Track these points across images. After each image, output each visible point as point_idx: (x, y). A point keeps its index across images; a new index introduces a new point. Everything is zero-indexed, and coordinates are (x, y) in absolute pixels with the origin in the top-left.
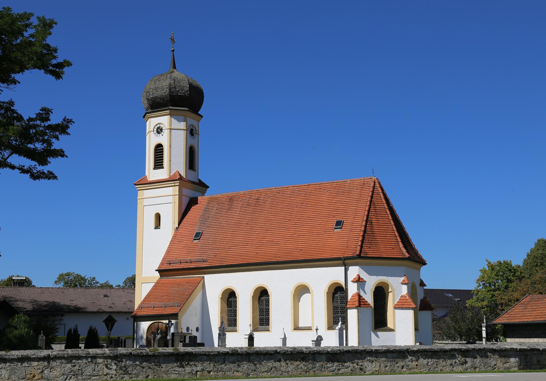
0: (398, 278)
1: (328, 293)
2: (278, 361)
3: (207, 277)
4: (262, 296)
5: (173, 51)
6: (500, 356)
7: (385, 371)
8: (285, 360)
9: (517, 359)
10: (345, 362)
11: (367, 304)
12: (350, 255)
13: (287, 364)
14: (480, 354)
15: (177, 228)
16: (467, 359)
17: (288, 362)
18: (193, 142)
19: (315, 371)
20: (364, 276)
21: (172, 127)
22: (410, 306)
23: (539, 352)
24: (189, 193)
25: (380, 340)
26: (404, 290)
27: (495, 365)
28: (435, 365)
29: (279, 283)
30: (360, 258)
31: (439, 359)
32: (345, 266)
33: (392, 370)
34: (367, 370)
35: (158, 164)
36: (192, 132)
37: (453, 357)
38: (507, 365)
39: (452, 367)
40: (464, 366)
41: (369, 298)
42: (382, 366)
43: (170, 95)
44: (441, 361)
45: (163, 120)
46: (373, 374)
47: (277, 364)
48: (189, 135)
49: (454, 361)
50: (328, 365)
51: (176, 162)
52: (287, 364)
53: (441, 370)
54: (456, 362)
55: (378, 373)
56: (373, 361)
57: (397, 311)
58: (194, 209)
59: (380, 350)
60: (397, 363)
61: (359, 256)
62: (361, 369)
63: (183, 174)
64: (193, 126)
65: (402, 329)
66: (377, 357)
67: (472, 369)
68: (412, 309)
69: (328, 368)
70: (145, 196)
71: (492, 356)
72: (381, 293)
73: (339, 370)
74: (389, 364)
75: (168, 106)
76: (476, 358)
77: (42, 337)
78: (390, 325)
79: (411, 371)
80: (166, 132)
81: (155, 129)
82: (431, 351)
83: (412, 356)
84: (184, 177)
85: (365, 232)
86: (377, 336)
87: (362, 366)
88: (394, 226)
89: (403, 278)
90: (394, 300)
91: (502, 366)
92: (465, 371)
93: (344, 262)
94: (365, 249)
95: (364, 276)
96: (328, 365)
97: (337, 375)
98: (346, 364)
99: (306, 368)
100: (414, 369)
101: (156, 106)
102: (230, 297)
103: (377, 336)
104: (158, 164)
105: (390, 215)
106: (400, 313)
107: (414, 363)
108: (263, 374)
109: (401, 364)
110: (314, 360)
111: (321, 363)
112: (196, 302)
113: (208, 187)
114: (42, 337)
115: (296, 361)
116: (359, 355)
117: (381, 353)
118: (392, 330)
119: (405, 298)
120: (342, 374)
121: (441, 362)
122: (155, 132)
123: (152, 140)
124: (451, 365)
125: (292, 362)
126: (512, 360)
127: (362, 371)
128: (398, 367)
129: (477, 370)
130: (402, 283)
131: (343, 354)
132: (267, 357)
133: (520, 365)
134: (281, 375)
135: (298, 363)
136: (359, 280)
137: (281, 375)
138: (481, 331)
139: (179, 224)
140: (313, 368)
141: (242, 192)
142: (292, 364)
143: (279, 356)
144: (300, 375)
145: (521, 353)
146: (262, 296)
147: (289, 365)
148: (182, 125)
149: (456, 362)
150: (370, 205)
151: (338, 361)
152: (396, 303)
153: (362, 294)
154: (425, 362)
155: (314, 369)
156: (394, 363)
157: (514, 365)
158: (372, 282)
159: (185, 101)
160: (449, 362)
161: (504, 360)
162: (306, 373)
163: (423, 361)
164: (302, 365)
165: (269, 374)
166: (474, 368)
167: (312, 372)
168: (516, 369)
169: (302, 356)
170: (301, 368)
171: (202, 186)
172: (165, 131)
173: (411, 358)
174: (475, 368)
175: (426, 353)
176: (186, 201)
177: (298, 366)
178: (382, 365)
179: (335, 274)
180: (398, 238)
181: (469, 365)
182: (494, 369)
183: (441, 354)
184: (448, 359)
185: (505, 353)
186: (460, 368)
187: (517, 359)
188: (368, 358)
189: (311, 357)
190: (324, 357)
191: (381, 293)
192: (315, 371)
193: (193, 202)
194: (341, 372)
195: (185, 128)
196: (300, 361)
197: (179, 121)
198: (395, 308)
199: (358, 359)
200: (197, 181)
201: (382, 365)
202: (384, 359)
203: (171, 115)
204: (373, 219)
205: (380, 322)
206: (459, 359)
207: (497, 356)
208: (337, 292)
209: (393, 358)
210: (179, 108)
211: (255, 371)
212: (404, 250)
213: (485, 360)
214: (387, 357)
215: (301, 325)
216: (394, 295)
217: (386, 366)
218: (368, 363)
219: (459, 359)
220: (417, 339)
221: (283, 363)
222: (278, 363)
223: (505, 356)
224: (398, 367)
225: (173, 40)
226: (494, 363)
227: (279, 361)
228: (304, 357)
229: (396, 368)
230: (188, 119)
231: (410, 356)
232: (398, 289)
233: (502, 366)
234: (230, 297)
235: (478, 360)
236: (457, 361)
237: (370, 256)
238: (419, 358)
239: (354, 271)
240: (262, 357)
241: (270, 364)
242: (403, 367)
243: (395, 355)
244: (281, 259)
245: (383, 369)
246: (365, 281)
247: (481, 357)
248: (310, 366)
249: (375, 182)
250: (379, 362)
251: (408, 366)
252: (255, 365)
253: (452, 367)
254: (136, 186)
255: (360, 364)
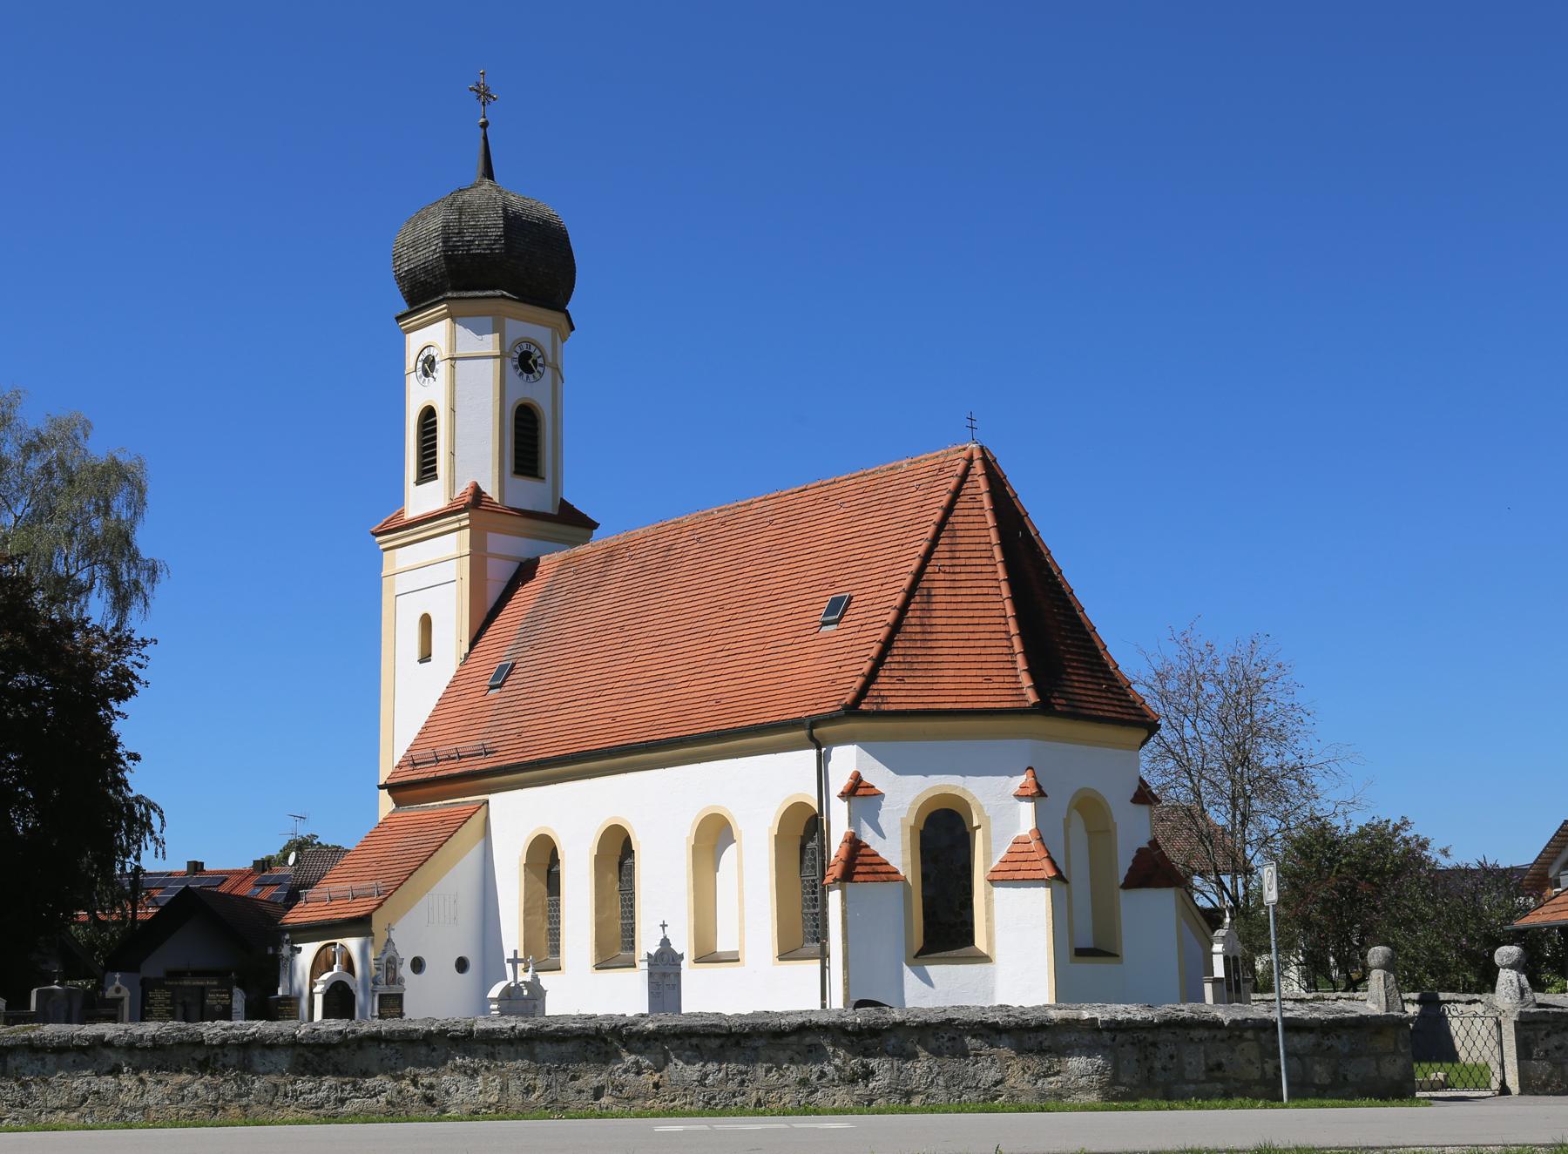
0: (919, 778)
1: (780, 840)
2: (110, 1073)
3: (497, 801)
4: (618, 853)
5: (485, 125)
6: (1022, 1051)
7: (525, 1105)
8: (137, 1070)
9: (1099, 1061)
10: (367, 1074)
11: (882, 872)
12: (828, 707)
13: (141, 1081)
14: (933, 1043)
15: (467, 656)
16: (874, 1063)
17: (145, 1075)
18: (536, 392)
19: (245, 1108)
20: (877, 775)
21: (460, 352)
22: (1039, 875)
23: (1220, 1034)
24: (509, 546)
25: (937, 990)
26: (1025, 818)
27: (997, 1083)
28: (732, 1086)
29: (657, 805)
30: (858, 714)
31: (753, 1061)
32: (819, 748)
33: (554, 1101)
34: (449, 1101)
35: (427, 471)
36: (526, 362)
37: (813, 1053)
38: (1052, 1084)
39: (805, 1091)
40: (860, 1089)
41: (895, 847)
42: (512, 1089)
43: (447, 257)
44: (760, 1070)
45: (433, 335)
46: (474, 1115)
47: (106, 1083)
48: (513, 374)
49: (816, 1069)
50: (299, 1086)
51: (475, 456)
52: (141, 1081)
53: (759, 1103)
54: (823, 1075)
55: (499, 1111)
56: (476, 1072)
57: (1000, 893)
58: (526, 595)
59: (501, 1031)
60: (574, 1078)
61: (852, 711)
62: (429, 1100)
63: (491, 489)
64: (530, 343)
65: (1016, 957)
66: (491, 1056)
67: (895, 1098)
68: (1046, 882)
69: (296, 1096)
70: (399, 567)
71: (986, 1050)
72: (945, 836)
73: (342, 1101)
74: (540, 1082)
75: (445, 291)
76: (913, 1056)
77: (118, 990)
78: (980, 942)
79: (630, 1104)
80: (442, 368)
81: (420, 365)
82: (717, 1036)
83: (640, 1053)
84: (496, 499)
85: (896, 627)
86: (927, 980)
87: (431, 1087)
88: (1008, 604)
89: (1022, 779)
90: (988, 856)
91: (1027, 1087)
92: (867, 1104)
93: (814, 732)
94: (883, 685)
95: (877, 775)
96: (299, 1086)
97: (332, 1118)
98: (369, 1083)
99: (212, 1096)
100: (646, 1098)
101: (421, 292)
102: (544, 861)
103: (927, 980)
104: (427, 471)
105: (1000, 568)
106: (1005, 896)
107: (648, 1079)
108: (52, 1117)
109: (591, 1079)
110: (246, 1067)
111: (274, 1078)
112: (452, 881)
113: (594, 525)
114: (118, 990)
115: (179, 1071)
116: (423, 1050)
117: (510, 1042)
118: (733, 958)
119: (1025, 848)
120: (354, 1118)
121: (761, 1071)
122: (420, 372)
123: (419, 394)
124: (804, 1082)
125: (161, 1075)
126: (1076, 1063)
127: (434, 1107)
128: (580, 1092)
129: (916, 1101)
130: (1019, 797)
131: (360, 1047)
132: (69, 1058)
133: (1115, 1081)
134: (116, 1118)
135: (185, 1078)
136: (856, 790)
137: (116, 1118)
138: (1209, 955)
139: (472, 645)
140: (239, 1096)
141: (640, 531)
142: (159, 1082)
143: (113, 1057)
144: (192, 1121)
145: (1120, 1037)
146: (618, 853)
147: (150, 1086)
148: (490, 343)
149: (823, 1075)
150: (935, 541)
151: (337, 1071)
152: (995, 863)
153: (868, 836)
154: (692, 1072)
155: (244, 1101)
156: (561, 1077)
157: (1083, 1081)
158: (904, 796)
159: (512, 269)
160: (794, 1073)
161: (1035, 1063)
162: (214, 1113)
163: (684, 1071)
164: (198, 1085)
165: (74, 1115)
166: (904, 1097)
167: (234, 1110)
168: (1094, 1098)
169: (200, 1055)
170: (196, 1095)
171: (571, 523)
172: (452, 370)
173: (632, 1058)
174: (908, 1095)
175: (695, 1041)
176: (500, 572)
177: (182, 1088)
178: (514, 1086)
179: (785, 776)
180: (1016, 641)
181: (881, 1081)
182: (990, 1099)
183: (760, 1043)
184: (792, 1061)
185: (1042, 1036)
186: (842, 1095)
187: (1099, 1061)
188: (459, 1061)
189: (233, 1058)
190: (283, 1059)
191: (945, 836)
192: (245, 1108)
193: (525, 571)
194: (348, 1108)
195: (497, 352)
196: (189, 1072)
197: (479, 332)
198: (993, 882)
199: (420, 1065)
200: (549, 507)
201: (514, 1086)
202: (520, 1064)
203: (453, 316)
204: (937, 581)
205: (947, 928)
206: (837, 1062)
207: (1006, 1051)
208: (803, 831)
209: (561, 1059)
210: (477, 293)
211: (23, 1105)
212: (1026, 681)
213: (953, 1065)
214: (533, 1057)
215: (722, 946)
216: (987, 840)
217: (529, 1090)
218: (457, 1077)
219: (837, 1062)
220: (1064, 991)
221: (128, 1081)
222: (109, 1078)
223: (1042, 1051)
224: (580, 1092)
225: (484, 95)
226: (993, 1074)
227: (115, 1071)
228: (207, 1059)
229: (571, 1094)
230: (509, 323)
231: (630, 1052)
232: (1004, 815)
233: (1027, 1087)
234: (544, 861)
235: (921, 1067)
236: (829, 1069)
237: (893, 707)
238: (667, 1061)
239: (846, 760)
240: (51, 1059)
241: (81, 1083)
242: (598, 1093)
243: (566, 1049)
244: (658, 735)
245: (517, 1100)
246: (880, 795)
247: (937, 1053)
248: (230, 1089)
249: (970, 460)
250: (501, 1075)
251: (620, 1088)
252: (25, 1086)
253: (805, 1091)
254: (378, 539)
255: (426, 1081)
